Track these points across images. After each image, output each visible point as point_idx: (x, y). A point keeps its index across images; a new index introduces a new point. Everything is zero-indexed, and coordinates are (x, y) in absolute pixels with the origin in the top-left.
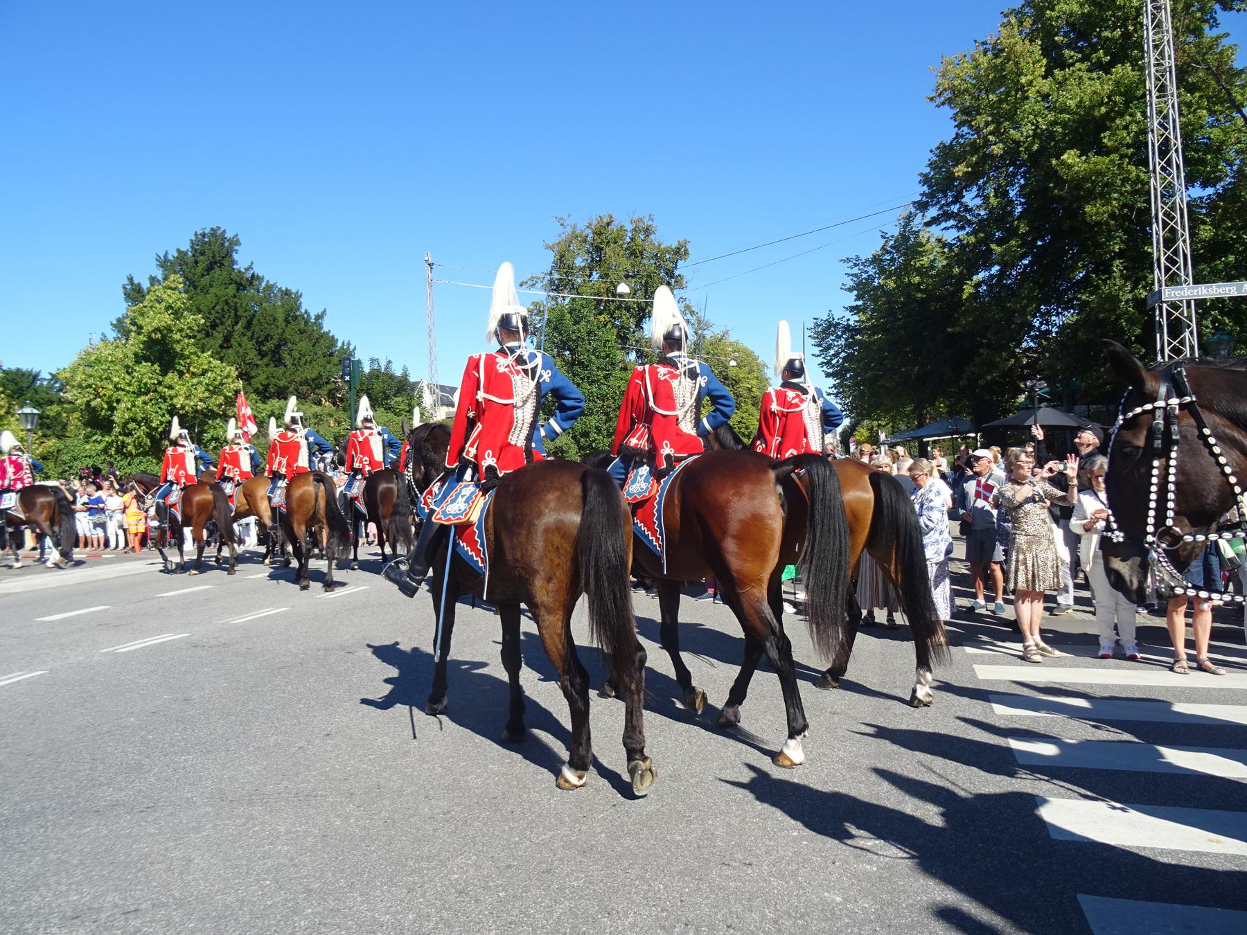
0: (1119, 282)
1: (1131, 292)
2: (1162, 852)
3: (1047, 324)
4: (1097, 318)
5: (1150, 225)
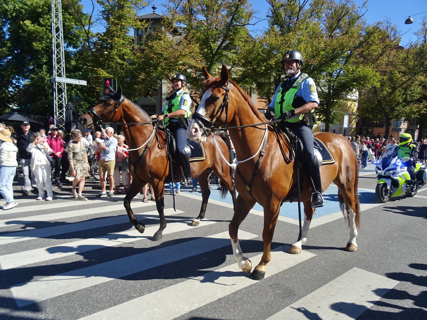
0: (45, 73)
1: (49, 77)
2: (43, 262)
3: (18, 83)
4: (37, 84)
5: (52, 55)
